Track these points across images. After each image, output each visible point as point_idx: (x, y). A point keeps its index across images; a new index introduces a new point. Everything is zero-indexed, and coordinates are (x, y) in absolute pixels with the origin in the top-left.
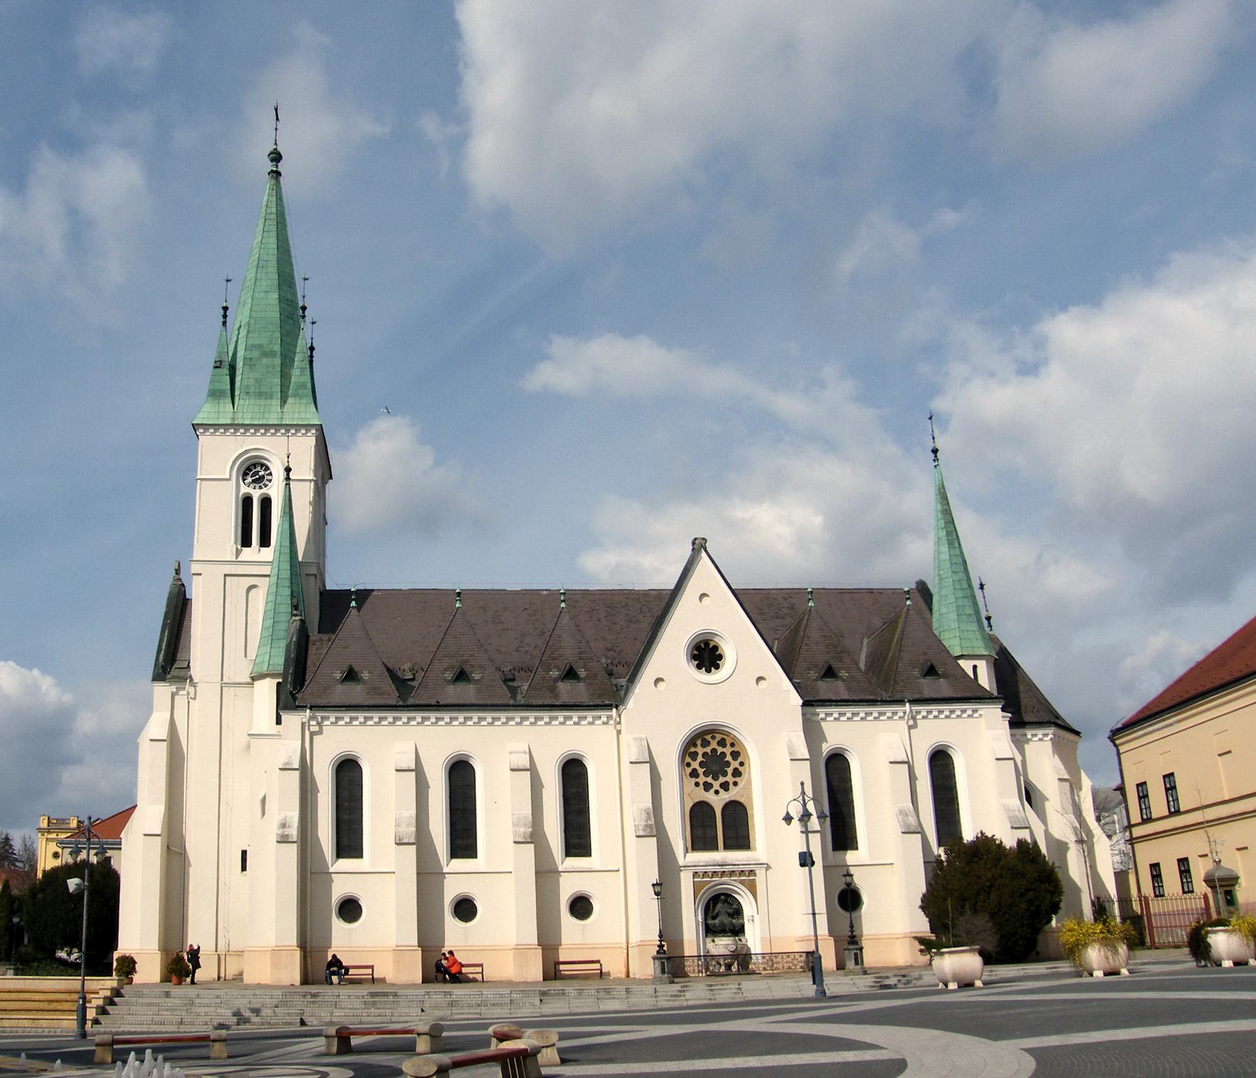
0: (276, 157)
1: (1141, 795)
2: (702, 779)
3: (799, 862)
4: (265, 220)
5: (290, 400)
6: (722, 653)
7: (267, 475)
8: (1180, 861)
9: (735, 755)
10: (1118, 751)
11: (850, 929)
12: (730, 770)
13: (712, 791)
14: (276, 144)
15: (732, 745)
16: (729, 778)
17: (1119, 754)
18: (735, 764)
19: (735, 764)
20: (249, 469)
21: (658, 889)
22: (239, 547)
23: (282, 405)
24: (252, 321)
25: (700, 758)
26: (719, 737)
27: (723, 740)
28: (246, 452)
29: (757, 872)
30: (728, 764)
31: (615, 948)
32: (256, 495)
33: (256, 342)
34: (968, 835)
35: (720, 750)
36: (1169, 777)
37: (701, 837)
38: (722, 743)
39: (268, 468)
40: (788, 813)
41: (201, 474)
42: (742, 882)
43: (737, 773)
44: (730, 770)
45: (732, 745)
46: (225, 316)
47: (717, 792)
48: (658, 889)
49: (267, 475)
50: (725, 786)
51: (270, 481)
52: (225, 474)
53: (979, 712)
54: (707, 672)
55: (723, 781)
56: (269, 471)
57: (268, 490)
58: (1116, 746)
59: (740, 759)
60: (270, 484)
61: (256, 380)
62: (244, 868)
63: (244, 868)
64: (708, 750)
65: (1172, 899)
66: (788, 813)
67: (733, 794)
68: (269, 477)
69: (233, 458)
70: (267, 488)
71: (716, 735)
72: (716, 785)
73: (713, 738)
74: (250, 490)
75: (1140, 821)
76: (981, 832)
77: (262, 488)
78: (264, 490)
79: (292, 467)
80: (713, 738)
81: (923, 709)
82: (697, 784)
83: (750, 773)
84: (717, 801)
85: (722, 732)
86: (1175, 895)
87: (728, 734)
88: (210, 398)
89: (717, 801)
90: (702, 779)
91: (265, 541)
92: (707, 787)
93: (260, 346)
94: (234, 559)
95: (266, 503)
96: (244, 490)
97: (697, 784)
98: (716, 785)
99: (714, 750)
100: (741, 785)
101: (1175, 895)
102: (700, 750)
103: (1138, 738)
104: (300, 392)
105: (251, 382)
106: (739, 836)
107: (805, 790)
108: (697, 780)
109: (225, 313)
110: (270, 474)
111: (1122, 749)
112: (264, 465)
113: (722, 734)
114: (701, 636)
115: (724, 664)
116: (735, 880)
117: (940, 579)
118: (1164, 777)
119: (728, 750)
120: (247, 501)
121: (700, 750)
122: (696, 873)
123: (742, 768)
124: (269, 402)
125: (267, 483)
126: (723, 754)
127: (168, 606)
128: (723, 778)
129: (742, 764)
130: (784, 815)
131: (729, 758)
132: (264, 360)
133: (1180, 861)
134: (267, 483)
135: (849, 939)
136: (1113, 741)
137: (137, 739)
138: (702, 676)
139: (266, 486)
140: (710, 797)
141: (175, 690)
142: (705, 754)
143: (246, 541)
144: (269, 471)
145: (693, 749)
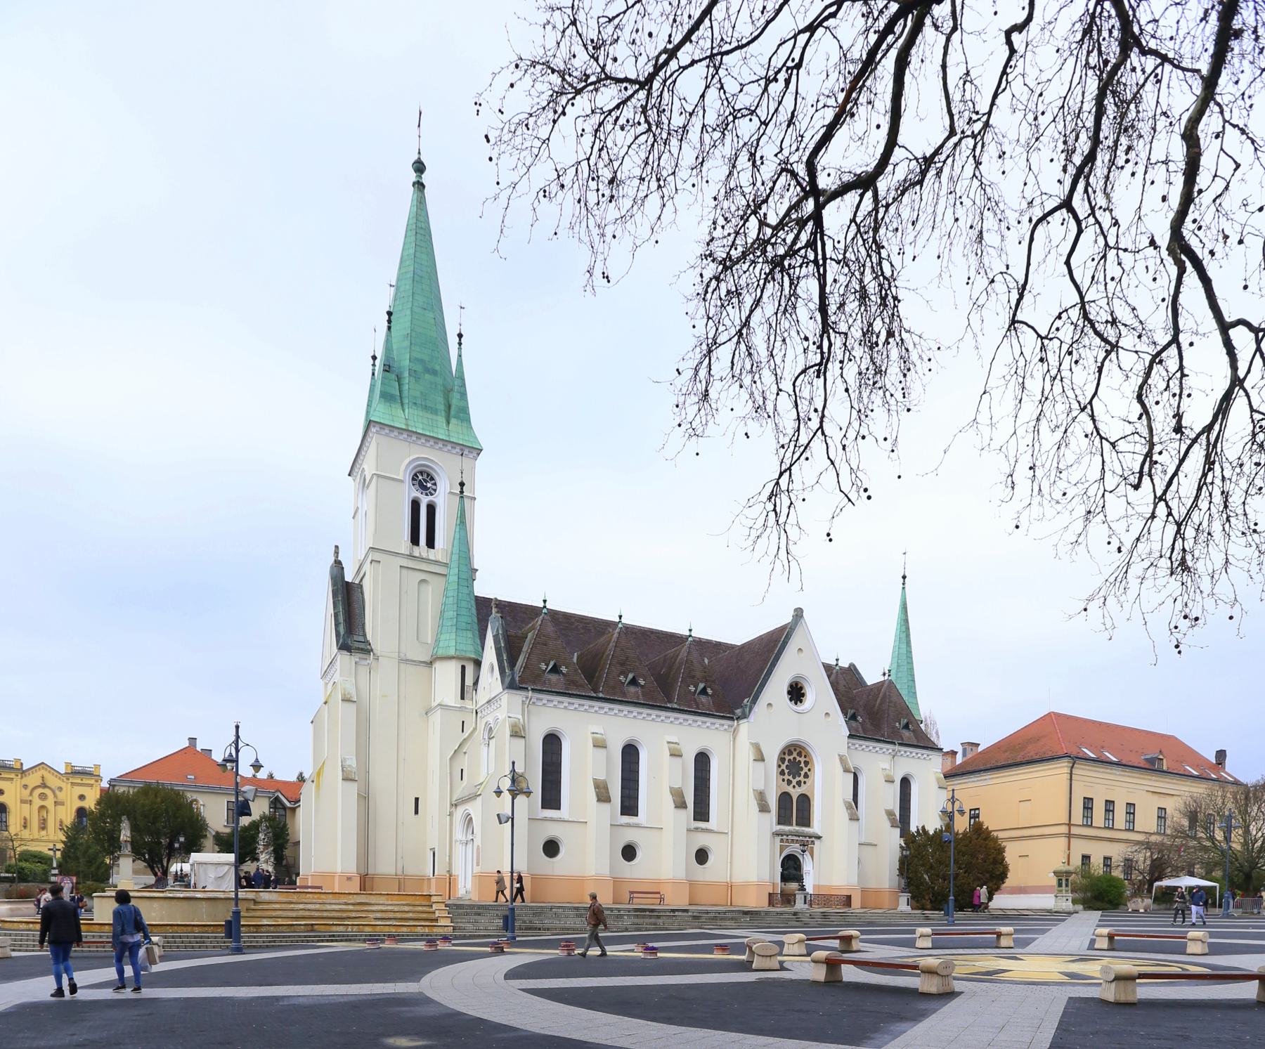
0: (419, 167)
2: (786, 777)
4: (514, 132)
5: (453, 421)
8: (1105, 858)
9: (806, 763)
12: (803, 773)
14: (419, 153)
15: (805, 756)
18: (805, 770)
23: (448, 422)
24: (414, 334)
25: (786, 763)
27: (800, 752)
28: (418, 459)
30: (802, 769)
32: (424, 501)
33: (420, 356)
34: (913, 829)
35: (798, 759)
36: (1131, 805)
38: (800, 754)
43: (806, 776)
45: (805, 756)
46: (389, 321)
50: (799, 783)
51: (435, 490)
52: (398, 475)
59: (780, 770)
61: (422, 393)
62: (416, 812)
63: (416, 812)
64: (791, 757)
68: (433, 492)
69: (411, 458)
72: (794, 782)
73: (795, 750)
76: (923, 827)
78: (430, 498)
81: (903, 749)
82: (805, 783)
84: (795, 793)
85: (800, 747)
88: (383, 400)
89: (795, 793)
90: (786, 777)
91: (431, 543)
92: (789, 782)
93: (421, 361)
95: (431, 509)
97: (783, 780)
100: (808, 784)
102: (795, 754)
104: (461, 415)
105: (418, 394)
106: (805, 820)
109: (389, 318)
110: (435, 484)
117: (898, 666)
118: (1106, 801)
119: (802, 759)
120: (415, 505)
121: (787, 758)
124: (435, 417)
125: (433, 492)
126: (800, 762)
127: (1181, 198)
129: (809, 770)
131: (803, 773)
132: (427, 376)
133: (1105, 858)
138: (792, 705)
139: (432, 494)
140: (790, 789)
142: (789, 760)
143: (415, 540)
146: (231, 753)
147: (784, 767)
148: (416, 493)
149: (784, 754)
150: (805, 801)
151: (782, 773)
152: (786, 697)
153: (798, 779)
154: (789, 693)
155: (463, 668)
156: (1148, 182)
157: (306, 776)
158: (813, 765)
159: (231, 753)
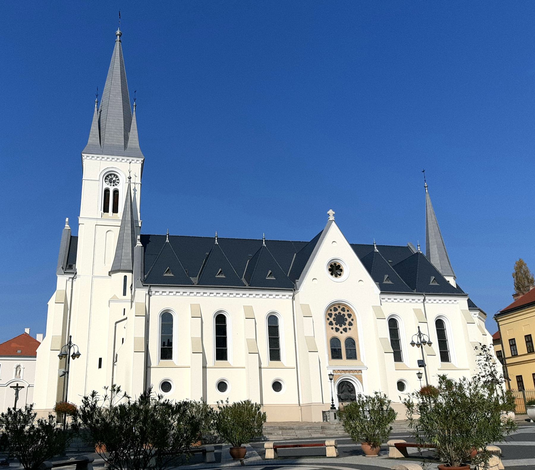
1: (511, 344)
3: (418, 365)
6: (342, 269)
7: (117, 180)
9: (349, 316)
10: (498, 324)
11: (332, 402)
13: (339, 332)
15: (348, 311)
16: (347, 326)
17: (499, 326)
18: (349, 320)
19: (347, 326)
20: (108, 176)
21: (331, 377)
22: (103, 212)
26: (341, 307)
27: (335, 308)
29: (362, 371)
31: (316, 405)
37: (336, 354)
38: (336, 309)
39: (117, 177)
40: (412, 341)
41: (85, 177)
42: (355, 376)
43: (350, 324)
44: (347, 323)
47: (341, 333)
48: (331, 377)
49: (117, 180)
51: (118, 183)
53: (457, 301)
54: (335, 277)
55: (344, 328)
56: (118, 178)
57: (117, 187)
58: (497, 322)
59: (352, 318)
60: (118, 185)
62: (124, 309)
63: (124, 309)
65: (530, 392)
66: (412, 341)
67: (348, 334)
68: (118, 181)
70: (117, 186)
71: (340, 306)
72: (341, 329)
73: (339, 307)
74: (108, 186)
75: (511, 356)
77: (114, 186)
78: (115, 187)
79: (131, 177)
80: (339, 307)
82: (350, 329)
83: (356, 324)
84: (343, 337)
85: (339, 305)
86: (532, 390)
87: (334, 305)
89: (343, 337)
90: (334, 326)
91: (115, 210)
92: (337, 330)
94: (101, 218)
95: (116, 192)
96: (106, 186)
98: (341, 329)
99: (340, 313)
100: (352, 329)
101: (532, 390)
103: (504, 320)
106: (352, 355)
107: (420, 330)
108: (332, 326)
110: (118, 180)
111: (500, 323)
112: (115, 175)
113: (343, 305)
114: (164, 311)
115: (343, 273)
116: (352, 375)
120: (107, 191)
122: (334, 370)
123: (353, 322)
125: (117, 184)
128: (339, 327)
129: (352, 320)
130: (411, 342)
134: (117, 184)
135: (331, 406)
136: (496, 319)
137: (48, 303)
139: (116, 185)
140: (337, 335)
141: (68, 279)
142: (335, 315)
143: (106, 210)
144: (118, 178)
145: (330, 312)
146: (418, 341)
147: (331, 319)
148: (106, 186)
149: (331, 310)
150: (351, 343)
151: (331, 324)
152: (328, 273)
153: (344, 327)
154: (330, 270)
155: (125, 277)
156: (107, 363)
157: (381, 306)
158: (355, 316)
159: (418, 341)
